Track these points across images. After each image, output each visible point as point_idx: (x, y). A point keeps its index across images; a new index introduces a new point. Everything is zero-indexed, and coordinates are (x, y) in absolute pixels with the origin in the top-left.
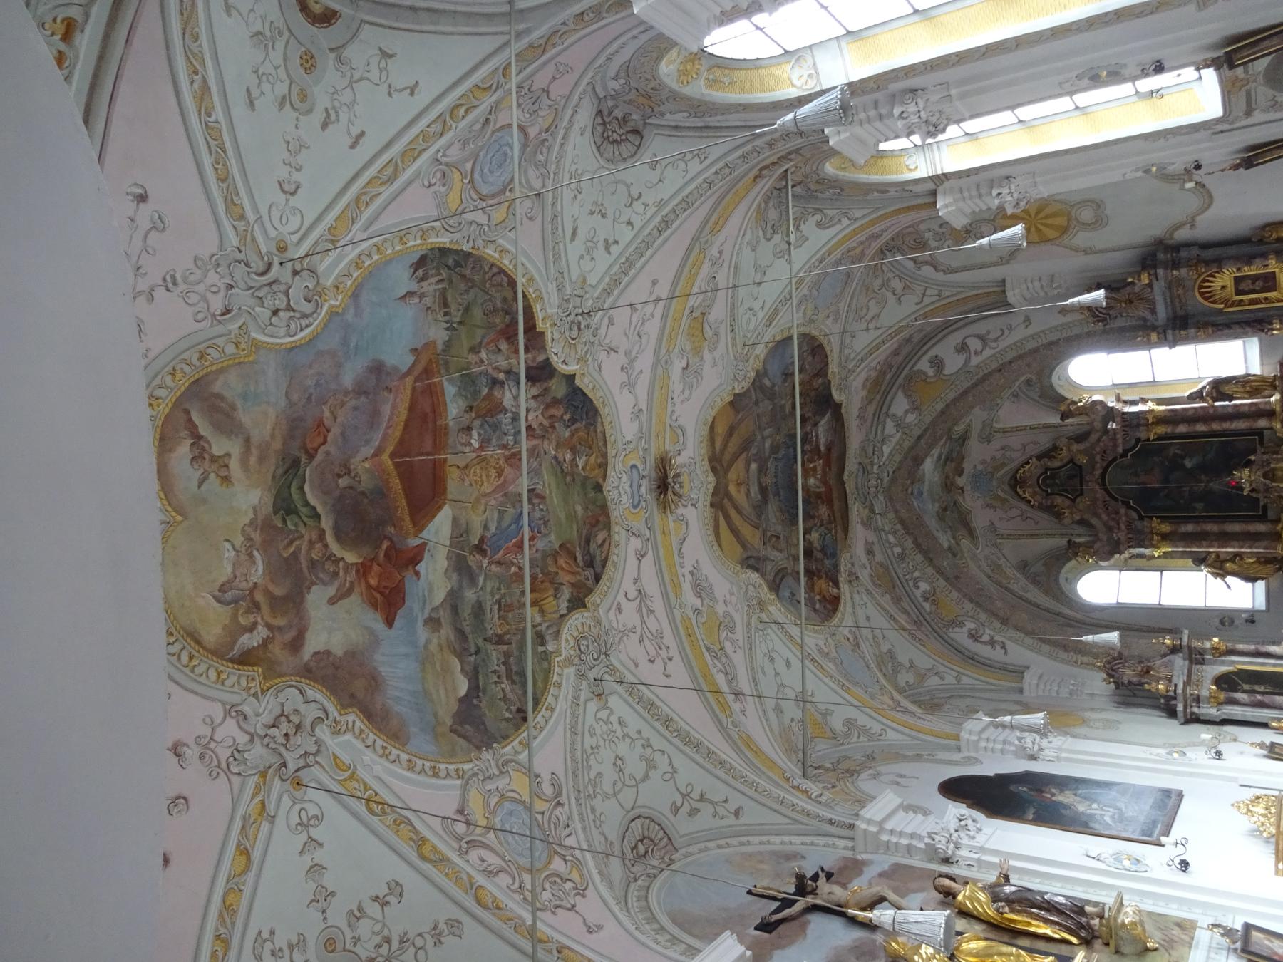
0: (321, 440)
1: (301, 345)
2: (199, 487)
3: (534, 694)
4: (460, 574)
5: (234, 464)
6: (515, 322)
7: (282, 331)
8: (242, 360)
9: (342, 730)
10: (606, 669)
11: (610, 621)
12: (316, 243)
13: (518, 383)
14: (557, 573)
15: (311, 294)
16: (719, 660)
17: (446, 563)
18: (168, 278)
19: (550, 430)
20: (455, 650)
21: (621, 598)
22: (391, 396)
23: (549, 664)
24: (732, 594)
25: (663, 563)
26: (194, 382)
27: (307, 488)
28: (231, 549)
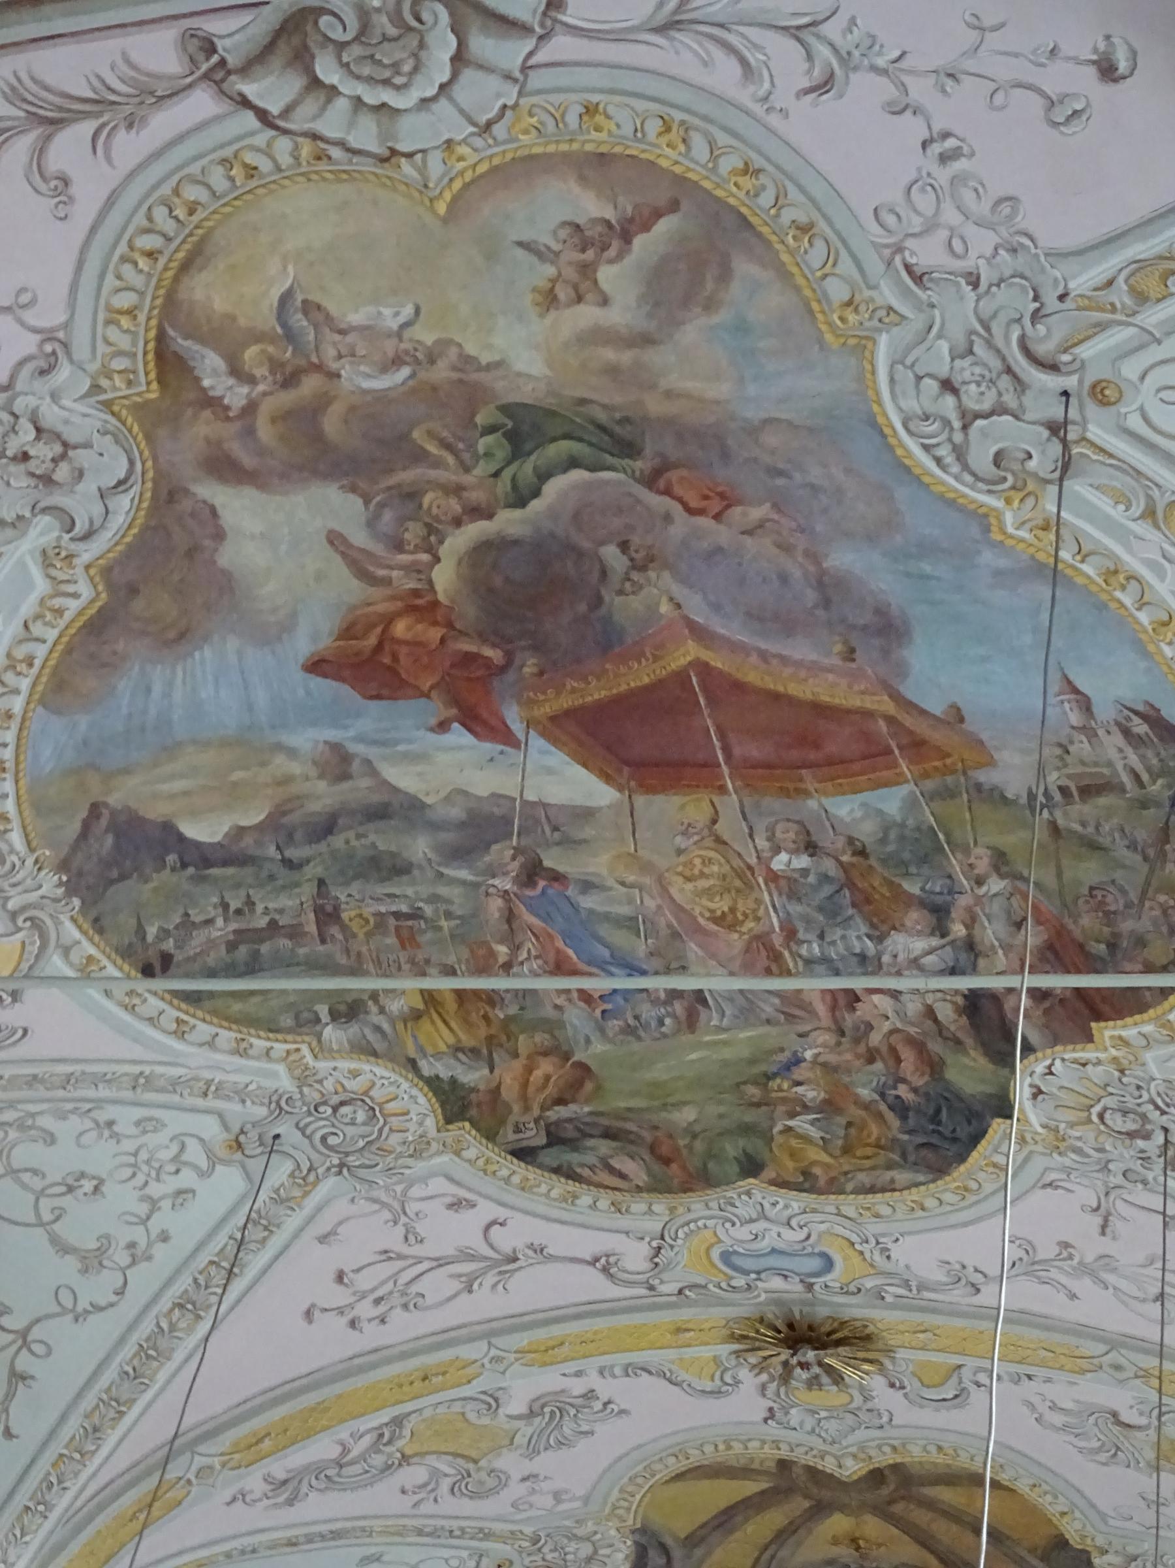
0: (694, 504)
1: (891, 449)
2: (520, 244)
3: (212, 995)
4: (462, 825)
5: (587, 315)
6: (1094, 965)
7: (911, 404)
8: (820, 316)
9: (54, 572)
10: (305, 1166)
11: (424, 1180)
12: (1139, 472)
13: (953, 971)
14: (516, 1055)
15: (1016, 467)
16: (375, 1448)
17: (485, 794)
18: (951, 143)
19: (862, 1049)
20: (284, 814)
21: (487, 1211)
22: (836, 661)
23: (289, 1031)
24: (557, 1496)
25: (600, 1323)
26: (744, 219)
27: (577, 475)
28: (401, 319)
